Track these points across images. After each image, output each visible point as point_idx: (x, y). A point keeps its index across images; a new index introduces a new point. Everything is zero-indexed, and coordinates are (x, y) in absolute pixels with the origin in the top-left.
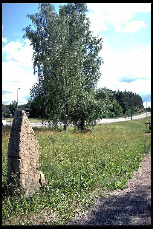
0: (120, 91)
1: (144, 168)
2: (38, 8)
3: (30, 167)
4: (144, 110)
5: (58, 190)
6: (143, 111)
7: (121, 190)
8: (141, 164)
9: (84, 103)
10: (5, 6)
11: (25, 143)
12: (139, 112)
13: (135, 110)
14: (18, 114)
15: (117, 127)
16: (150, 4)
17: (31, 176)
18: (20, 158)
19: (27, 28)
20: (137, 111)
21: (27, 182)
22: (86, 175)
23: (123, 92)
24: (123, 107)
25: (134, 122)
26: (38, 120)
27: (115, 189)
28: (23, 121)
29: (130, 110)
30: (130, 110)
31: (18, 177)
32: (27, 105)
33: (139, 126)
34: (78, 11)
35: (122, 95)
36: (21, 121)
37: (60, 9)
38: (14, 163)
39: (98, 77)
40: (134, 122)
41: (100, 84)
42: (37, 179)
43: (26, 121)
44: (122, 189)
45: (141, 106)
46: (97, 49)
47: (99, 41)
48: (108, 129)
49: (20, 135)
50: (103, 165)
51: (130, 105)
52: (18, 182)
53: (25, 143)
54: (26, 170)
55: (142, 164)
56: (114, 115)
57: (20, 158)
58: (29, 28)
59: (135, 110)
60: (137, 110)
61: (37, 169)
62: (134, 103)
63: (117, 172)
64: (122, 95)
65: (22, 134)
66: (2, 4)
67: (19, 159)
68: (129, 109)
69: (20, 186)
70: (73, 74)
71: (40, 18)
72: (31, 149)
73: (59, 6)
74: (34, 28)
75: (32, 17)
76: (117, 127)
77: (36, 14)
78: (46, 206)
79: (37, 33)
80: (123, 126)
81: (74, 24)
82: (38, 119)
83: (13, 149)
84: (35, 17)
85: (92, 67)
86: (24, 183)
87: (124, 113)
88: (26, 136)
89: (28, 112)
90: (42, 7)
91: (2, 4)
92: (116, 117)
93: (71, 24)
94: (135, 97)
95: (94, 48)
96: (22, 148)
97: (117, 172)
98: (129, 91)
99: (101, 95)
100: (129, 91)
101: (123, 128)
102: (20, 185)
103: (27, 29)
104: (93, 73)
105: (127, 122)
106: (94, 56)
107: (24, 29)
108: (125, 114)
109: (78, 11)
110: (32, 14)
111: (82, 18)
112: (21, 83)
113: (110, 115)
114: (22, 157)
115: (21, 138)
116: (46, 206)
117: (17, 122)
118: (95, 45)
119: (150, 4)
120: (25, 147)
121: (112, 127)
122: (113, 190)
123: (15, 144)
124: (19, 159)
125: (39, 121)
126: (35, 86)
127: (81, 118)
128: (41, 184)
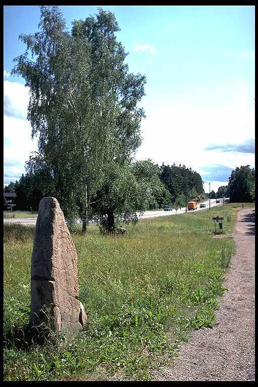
0: (166, 164)
1: (231, 292)
2: (39, 25)
3: (67, 295)
4: (204, 196)
5: (110, 332)
6: (203, 199)
7: (209, 329)
8: (223, 286)
9: (116, 187)
10: (8, 9)
11: (60, 253)
12: (197, 199)
13: (191, 195)
14: (46, 204)
15: (166, 224)
16: (254, 7)
17: (67, 310)
18: (53, 280)
19: (21, 58)
20: (194, 198)
21: (63, 320)
22: (150, 303)
23: (170, 167)
24: (171, 192)
25: (191, 215)
26: (29, 214)
27: (200, 327)
28: (56, 216)
29: (182, 196)
30: (182, 196)
31: (52, 313)
32: (8, 188)
33: (200, 223)
34: (103, 31)
35: (168, 172)
36: (52, 216)
37: (73, 27)
38: (43, 288)
39: (136, 143)
40: (191, 215)
41: (139, 155)
42: (77, 316)
43: (59, 216)
44: (211, 328)
45: (200, 190)
46: (138, 95)
47: (139, 82)
48: (151, 229)
49: (52, 241)
50: (168, 289)
51: (183, 187)
52: (52, 321)
53: (60, 253)
54: (61, 299)
55: (226, 286)
56: (157, 205)
57: (53, 280)
58: (24, 57)
59: (191, 195)
60: (194, 196)
61: (76, 297)
62: (188, 185)
63: (194, 300)
64: (168, 172)
65: (55, 238)
66: (4, 6)
67: (52, 282)
68: (181, 194)
69: (54, 327)
70: (99, 136)
71: (42, 40)
72: (68, 264)
73: (72, 22)
74: (33, 59)
75: (28, 40)
76: (166, 224)
77: (36, 35)
78: (102, 360)
79: (37, 66)
80: (175, 223)
81: (97, 52)
82: (28, 212)
83: (41, 264)
84: (34, 39)
85: (128, 130)
86: (59, 322)
87: (173, 201)
88: (60, 242)
89: (11, 201)
90: (45, 23)
91: (4, 6)
92: (159, 208)
93: (93, 51)
94: (191, 175)
95: (131, 94)
96: (56, 263)
97: (194, 300)
98: (180, 165)
99: (143, 171)
100: (180, 165)
101: (176, 226)
102: (54, 326)
103: (21, 59)
104: (129, 134)
105: (180, 215)
106: (130, 107)
107: (16, 60)
108: (174, 202)
109: (103, 31)
110: (28, 34)
111: (112, 42)
112: (22, 149)
113: (150, 205)
114: (55, 278)
115: (54, 245)
116: (102, 360)
117: (47, 218)
118: (134, 87)
119: (254, 7)
120: (60, 260)
121: (158, 225)
122: (198, 330)
123: (45, 255)
124: (52, 282)
125: (31, 215)
126: (34, 156)
127: (108, 208)
128: (81, 321)
